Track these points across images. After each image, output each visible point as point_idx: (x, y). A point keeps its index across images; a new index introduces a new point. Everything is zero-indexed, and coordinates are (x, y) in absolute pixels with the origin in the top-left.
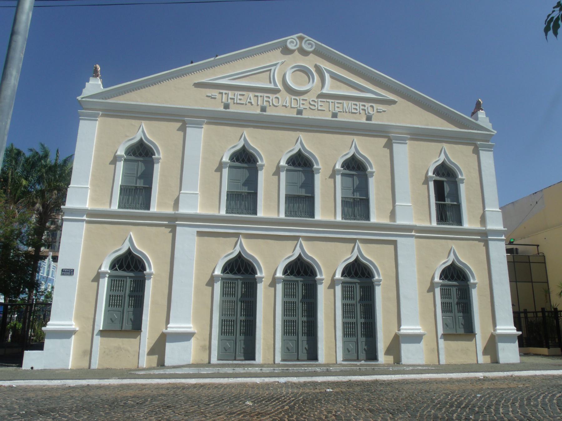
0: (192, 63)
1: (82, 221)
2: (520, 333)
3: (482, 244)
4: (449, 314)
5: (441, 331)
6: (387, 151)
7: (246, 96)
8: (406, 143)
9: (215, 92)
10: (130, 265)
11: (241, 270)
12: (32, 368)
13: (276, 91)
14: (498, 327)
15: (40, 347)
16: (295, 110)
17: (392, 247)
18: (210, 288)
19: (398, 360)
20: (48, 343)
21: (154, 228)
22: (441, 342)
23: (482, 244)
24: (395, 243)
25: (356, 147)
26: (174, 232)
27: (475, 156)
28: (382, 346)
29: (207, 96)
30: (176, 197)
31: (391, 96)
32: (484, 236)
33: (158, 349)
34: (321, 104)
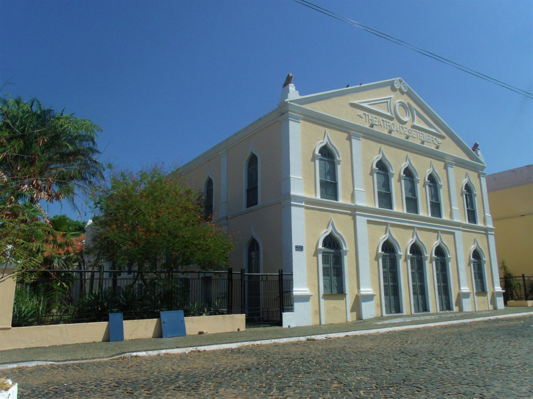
0: (348, 86)
1: (459, 230)
2: (504, 291)
3: (351, 217)
4: (327, 278)
5: (322, 293)
6: (348, 142)
7: (378, 119)
8: (299, 122)
9: (361, 113)
10: (332, 242)
11: (389, 248)
12: (289, 326)
13: (391, 119)
14: (361, 289)
15: (291, 310)
16: (405, 136)
17: (452, 236)
18: (315, 258)
19: (461, 310)
20: (297, 305)
21: (343, 215)
22: (322, 301)
23: (351, 217)
24: (453, 234)
25: (328, 137)
26: (487, 238)
27: (445, 171)
28: (454, 300)
29: (358, 115)
30: (351, 193)
31: (444, 134)
32: (486, 231)
33: (357, 308)
34: (414, 133)
